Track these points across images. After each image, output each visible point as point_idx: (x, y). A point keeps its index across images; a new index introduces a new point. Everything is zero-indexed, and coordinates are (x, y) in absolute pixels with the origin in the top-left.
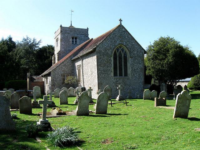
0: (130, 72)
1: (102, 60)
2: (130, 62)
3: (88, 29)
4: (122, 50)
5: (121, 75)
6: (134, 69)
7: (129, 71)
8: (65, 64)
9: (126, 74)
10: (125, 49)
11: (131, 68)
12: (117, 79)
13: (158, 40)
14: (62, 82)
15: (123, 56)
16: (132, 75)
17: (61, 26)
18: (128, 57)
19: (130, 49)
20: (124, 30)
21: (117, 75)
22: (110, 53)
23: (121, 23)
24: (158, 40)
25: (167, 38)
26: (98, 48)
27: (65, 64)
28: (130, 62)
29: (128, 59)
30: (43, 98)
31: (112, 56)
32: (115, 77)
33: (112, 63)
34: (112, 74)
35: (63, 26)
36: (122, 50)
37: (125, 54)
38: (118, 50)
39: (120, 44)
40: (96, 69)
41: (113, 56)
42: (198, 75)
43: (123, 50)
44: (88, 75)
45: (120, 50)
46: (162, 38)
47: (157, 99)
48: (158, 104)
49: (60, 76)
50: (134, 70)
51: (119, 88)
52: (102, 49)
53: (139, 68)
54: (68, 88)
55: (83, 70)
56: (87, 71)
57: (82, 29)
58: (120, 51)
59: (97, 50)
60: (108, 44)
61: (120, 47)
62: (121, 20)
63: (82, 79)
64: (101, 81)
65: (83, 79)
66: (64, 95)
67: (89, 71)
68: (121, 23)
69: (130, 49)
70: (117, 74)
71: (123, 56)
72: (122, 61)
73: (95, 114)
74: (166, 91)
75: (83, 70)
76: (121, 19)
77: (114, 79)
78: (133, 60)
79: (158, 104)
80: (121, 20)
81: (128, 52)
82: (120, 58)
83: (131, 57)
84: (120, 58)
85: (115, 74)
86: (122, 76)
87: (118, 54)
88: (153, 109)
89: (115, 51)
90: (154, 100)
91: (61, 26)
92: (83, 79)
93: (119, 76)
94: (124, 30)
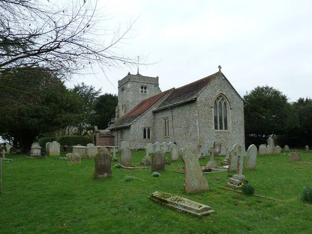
3: (158, 78)
5: (221, 128)
7: (229, 124)
21: (222, 129)
23: (220, 70)
28: (230, 113)
52: (202, 99)
62: (220, 67)
68: (220, 70)
80: (220, 67)
85: (216, 128)
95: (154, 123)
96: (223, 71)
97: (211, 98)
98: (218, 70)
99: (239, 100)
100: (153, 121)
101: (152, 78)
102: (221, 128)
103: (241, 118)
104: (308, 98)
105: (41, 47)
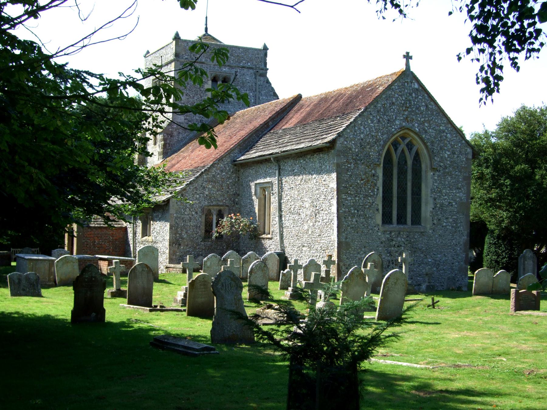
0: (428, 214)
1: (351, 176)
2: (430, 181)
3: (265, 49)
4: (407, 145)
5: (401, 220)
6: (442, 205)
7: (427, 210)
8: (214, 176)
9: (417, 220)
10: (419, 145)
11: (431, 201)
12: (391, 232)
13: (513, 115)
14: (202, 231)
15: (410, 162)
16: (435, 222)
17: (177, 38)
18: (423, 166)
19: (432, 142)
20: (416, 86)
21: (405, 223)
22: (373, 154)
23: (407, 65)
24: (513, 115)
25: (541, 110)
26: (342, 139)
27: (214, 176)
28: (430, 181)
29: (423, 173)
30: (247, 282)
31: (379, 165)
32: (388, 227)
33: (380, 183)
34: (379, 218)
35: (183, 37)
36: (407, 145)
37: (417, 158)
38: (395, 144)
39: (402, 128)
40: (334, 202)
41: (382, 165)
42: (545, 344)
43: (410, 146)
44: (303, 216)
45: (403, 146)
46: (524, 108)
47: (517, 293)
48: (519, 307)
49: (196, 213)
50: (439, 208)
51: (403, 260)
52: (352, 144)
53: (455, 201)
54: (222, 255)
55: (280, 198)
56: (300, 203)
57: (246, 50)
58: (403, 151)
59: (338, 145)
60: (370, 128)
61: (403, 138)
62: (408, 57)
63: (275, 227)
64: (346, 238)
65: (281, 226)
66: (260, 274)
67: (307, 205)
68: (407, 65)
69: (432, 142)
70: (391, 217)
71: (410, 162)
72: (406, 178)
73: (375, 321)
74: (534, 273)
75: (280, 198)
76: (408, 53)
77: (384, 232)
78: (439, 176)
79: (519, 307)
80: (408, 57)
81: (424, 152)
82: (402, 172)
83: (433, 169)
84: (402, 172)
85: (387, 219)
86: (405, 223)
87: (395, 159)
88: (508, 316)
89: (388, 150)
90: (507, 296)
91: (177, 38)
92: (281, 226)
93: (412, 224)
94: (416, 86)
95: (237, 195)
96: (414, 69)
97: (378, 140)
98: (402, 67)
99: (165, 72)
100: (232, 191)
101: (383, 219)
102: (401, 220)
103: (411, 170)
104: (498, 123)
105: (161, 67)
